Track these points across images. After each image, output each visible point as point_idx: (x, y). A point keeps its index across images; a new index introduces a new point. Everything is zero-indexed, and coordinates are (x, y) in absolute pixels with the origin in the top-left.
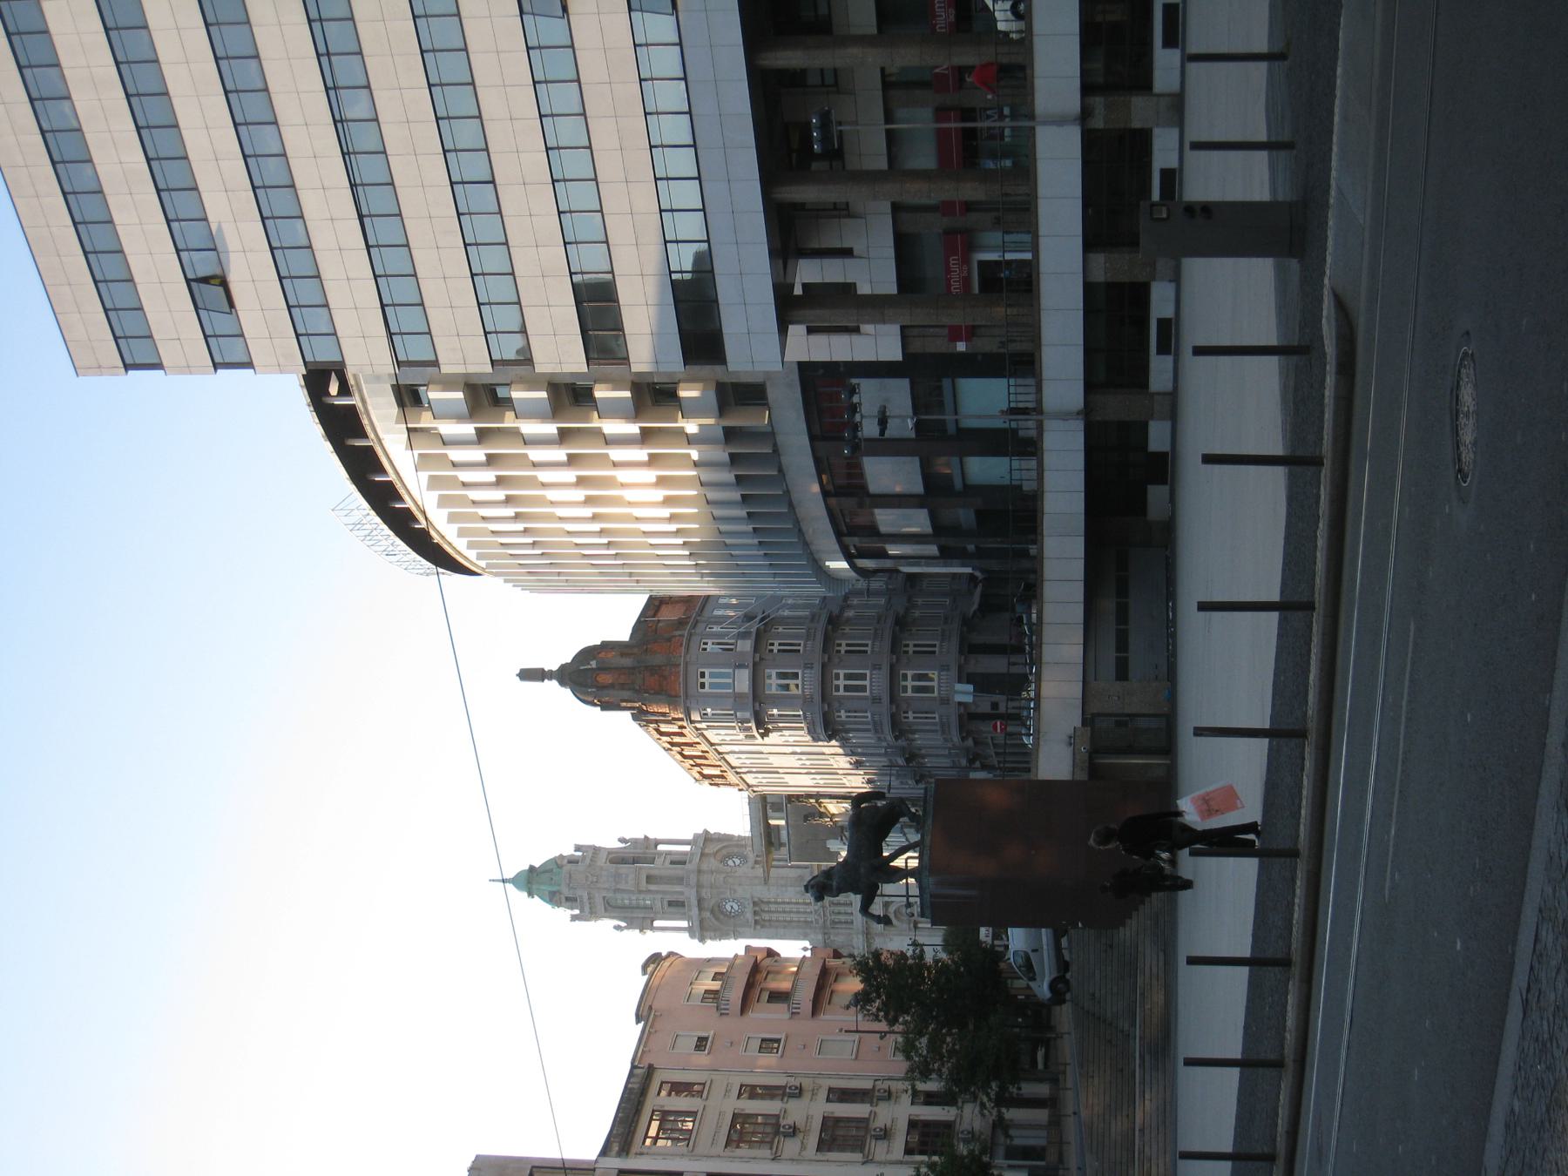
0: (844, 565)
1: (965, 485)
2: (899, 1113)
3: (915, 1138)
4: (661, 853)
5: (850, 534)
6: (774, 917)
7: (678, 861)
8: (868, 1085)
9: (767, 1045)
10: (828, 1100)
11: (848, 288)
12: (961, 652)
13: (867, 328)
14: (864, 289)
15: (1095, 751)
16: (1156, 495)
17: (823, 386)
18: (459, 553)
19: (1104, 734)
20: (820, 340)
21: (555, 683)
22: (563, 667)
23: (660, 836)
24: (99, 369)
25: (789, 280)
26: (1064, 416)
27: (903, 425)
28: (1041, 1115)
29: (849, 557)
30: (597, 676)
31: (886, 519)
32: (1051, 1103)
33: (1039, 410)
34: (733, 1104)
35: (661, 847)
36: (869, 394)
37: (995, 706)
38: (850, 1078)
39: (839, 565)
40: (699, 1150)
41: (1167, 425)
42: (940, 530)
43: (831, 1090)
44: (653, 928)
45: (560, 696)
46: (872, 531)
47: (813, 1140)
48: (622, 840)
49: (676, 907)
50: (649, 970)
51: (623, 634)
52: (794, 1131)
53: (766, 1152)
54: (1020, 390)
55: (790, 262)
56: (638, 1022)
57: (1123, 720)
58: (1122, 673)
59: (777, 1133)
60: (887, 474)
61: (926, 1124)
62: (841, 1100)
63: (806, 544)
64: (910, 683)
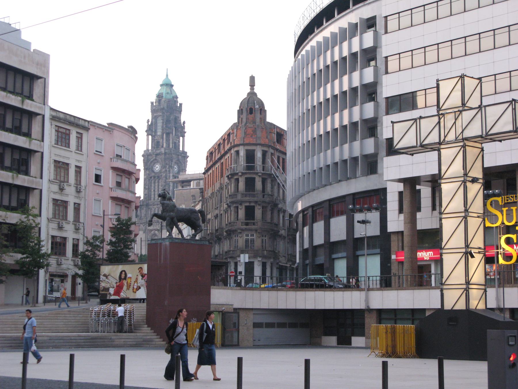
0: (300, 208)
1: (334, 259)
2: (69, 233)
3: (58, 240)
4: (179, 139)
5: (313, 211)
7: (176, 145)
8: (81, 220)
9: (98, 178)
10: (75, 204)
11: (419, 210)
13: (402, 216)
14: (419, 215)
16: (333, 340)
17: (376, 198)
18: (304, 47)
19: (231, 317)
20: (396, 197)
21: (249, 90)
22: (255, 94)
23: (185, 138)
25: (422, 183)
26: (367, 301)
27: (360, 231)
28: (69, 294)
29: (303, 211)
30: (252, 108)
32: (73, 297)
33: (369, 289)
35: (181, 138)
36: (374, 216)
37: (241, 273)
38: (84, 213)
39: (300, 206)
40: (53, 149)
41: (363, 345)
43: (79, 204)
44: (148, 135)
45: (243, 93)
46: (314, 220)
48: (184, 123)
49: (156, 144)
50: (130, 129)
51: (270, 119)
52: (62, 189)
53: (52, 177)
54: (375, 282)
55: (430, 184)
56: (108, 124)
57: (236, 326)
58: (256, 325)
59: (61, 182)
60: (338, 228)
61: (65, 245)
62: (75, 208)
63: (309, 192)
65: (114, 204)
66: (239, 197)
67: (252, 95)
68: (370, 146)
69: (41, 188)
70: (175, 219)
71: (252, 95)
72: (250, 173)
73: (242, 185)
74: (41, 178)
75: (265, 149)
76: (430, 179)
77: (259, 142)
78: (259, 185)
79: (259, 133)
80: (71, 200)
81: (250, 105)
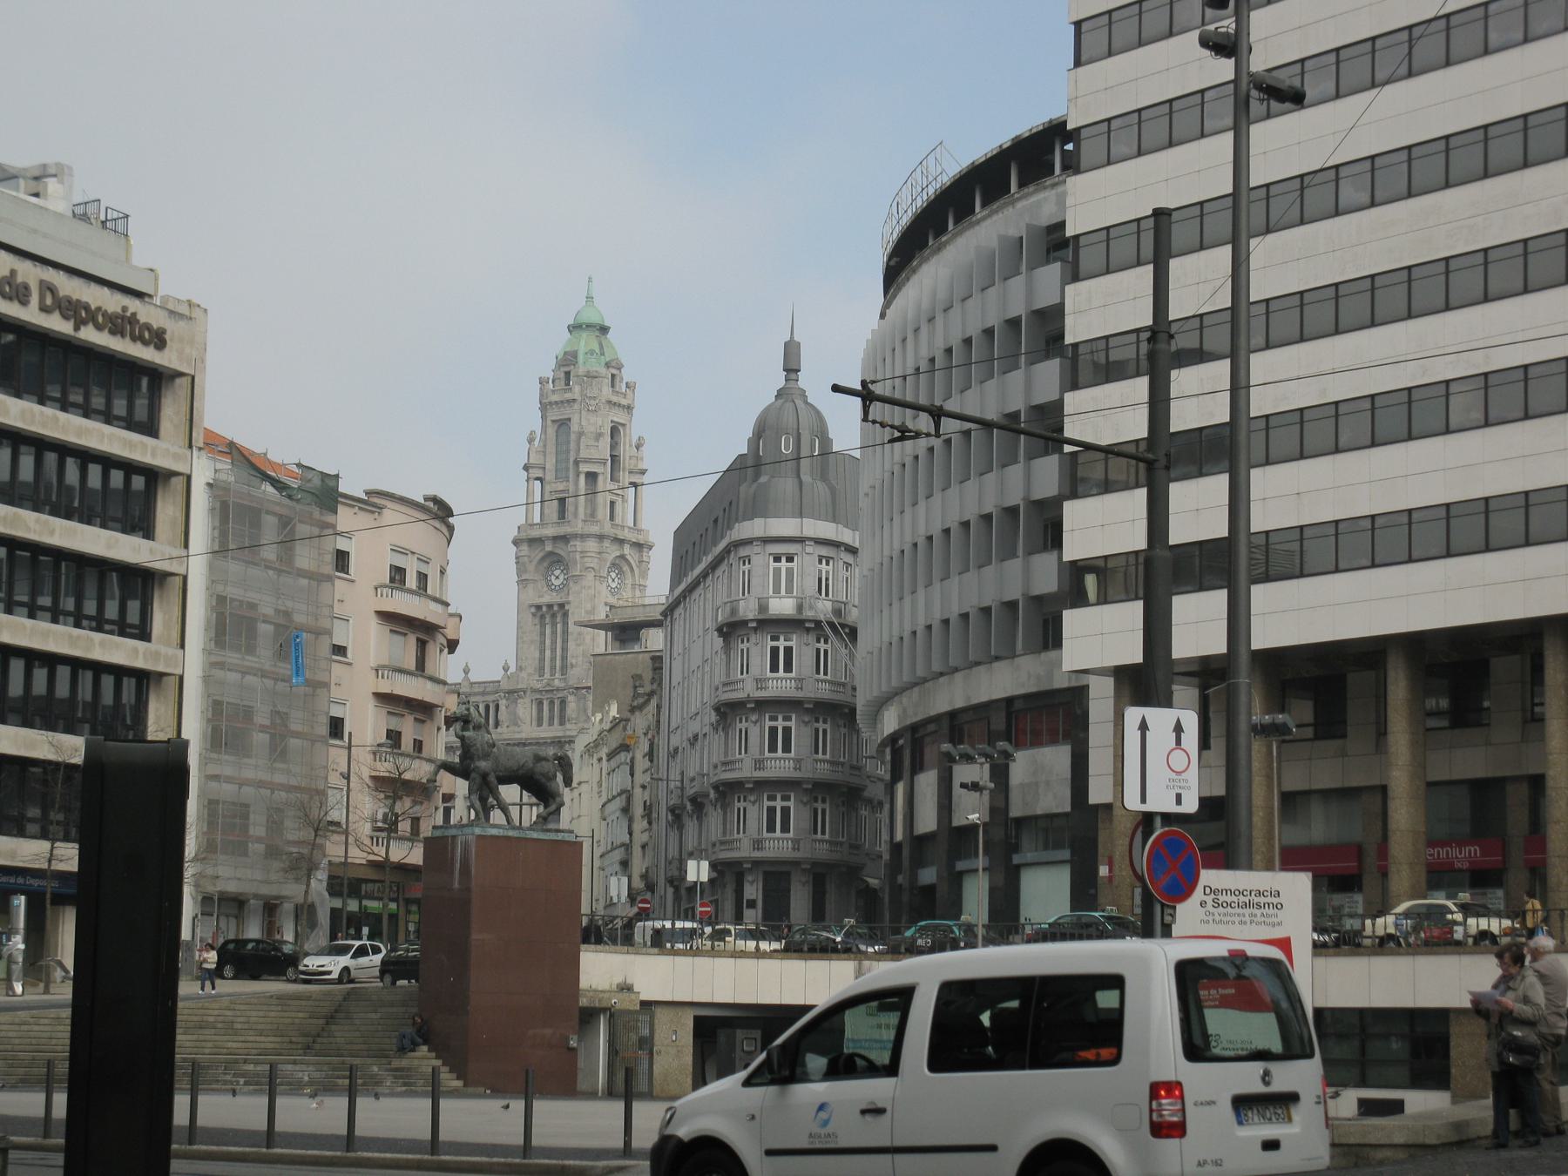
1: (1018, 867)
6: (548, 631)
12: (815, 864)
15: (612, 1014)
21: (781, 383)
31: (927, 782)
42: (921, 843)
46: (918, 767)
50: (431, 504)
55: (1196, 680)
56: (368, 493)
57: (646, 1044)
64: (779, 804)
65: (384, 711)
68: (1045, 576)
69: (178, 671)
70: (492, 778)
76: (1194, 668)
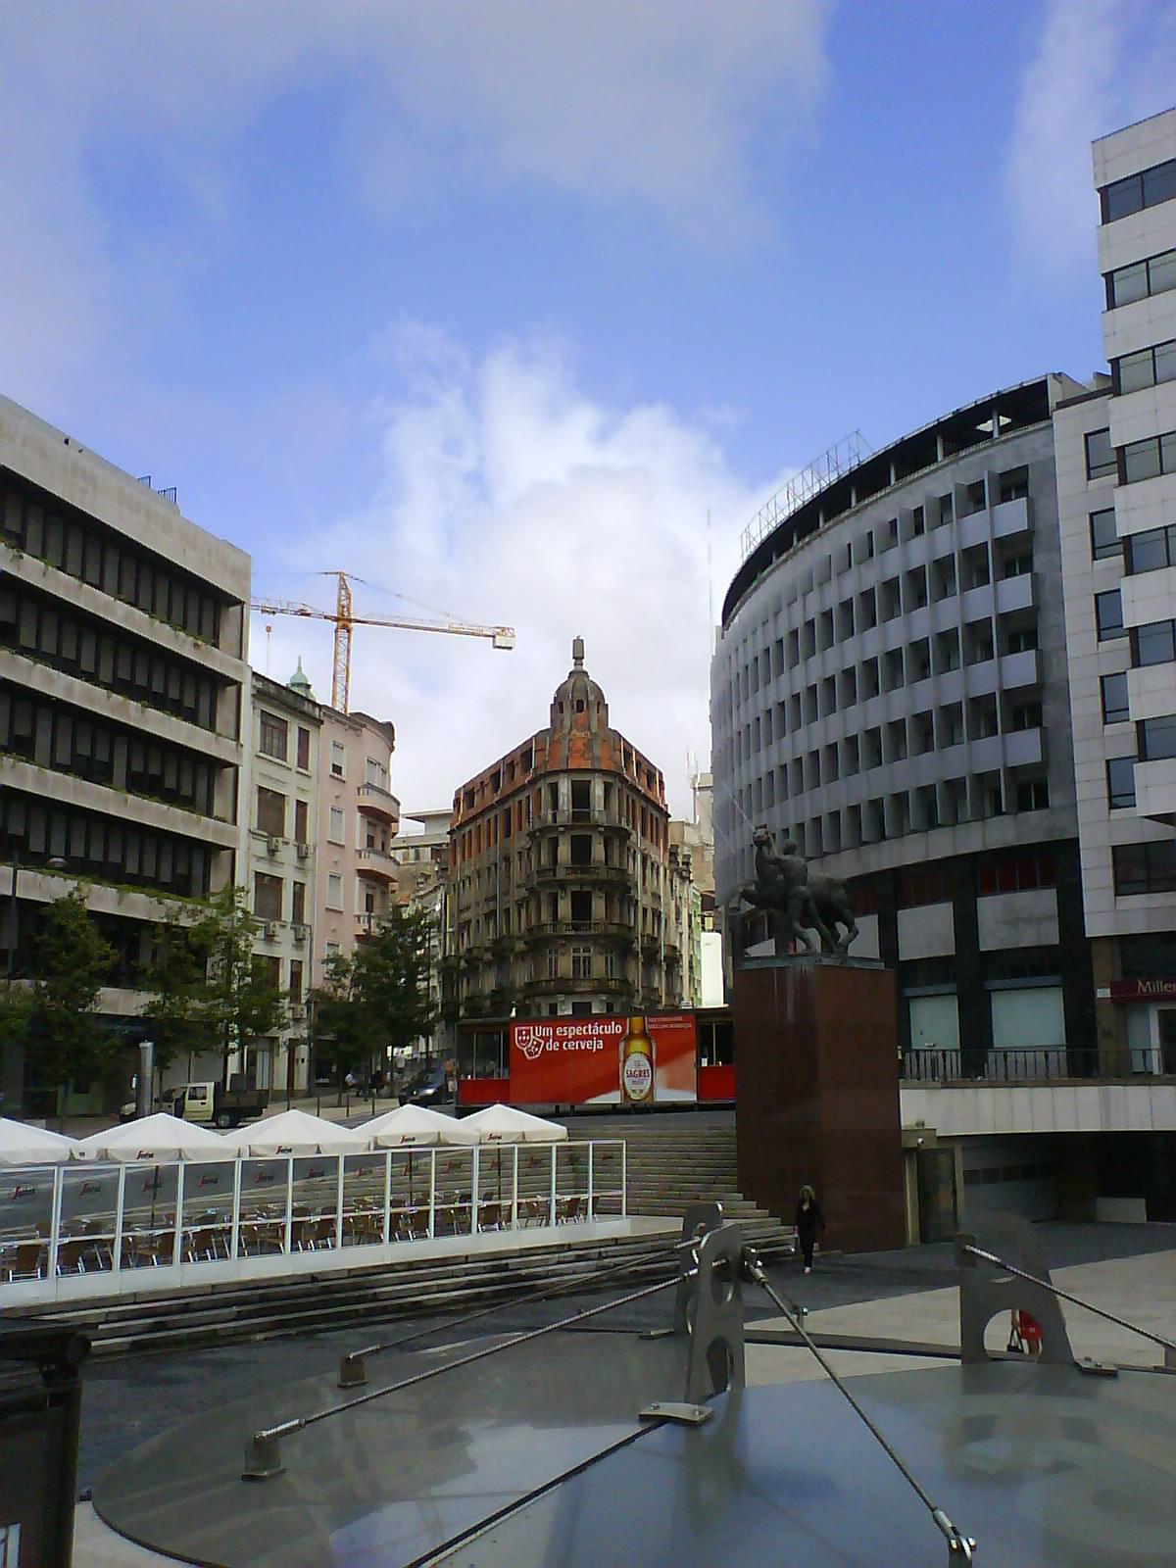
10: (295, 883)
24: (1101, 162)
27: (911, 948)
34: (292, 796)
43: (303, 885)
47: (264, 868)
52: (272, 852)
60: (926, 930)
66: (561, 874)
67: (578, 674)
71: (578, 674)
72: (581, 827)
73: (564, 851)
74: (235, 822)
75: (609, 780)
77: (597, 767)
78: (598, 851)
79: (598, 751)
80: (289, 874)
81: (579, 696)
